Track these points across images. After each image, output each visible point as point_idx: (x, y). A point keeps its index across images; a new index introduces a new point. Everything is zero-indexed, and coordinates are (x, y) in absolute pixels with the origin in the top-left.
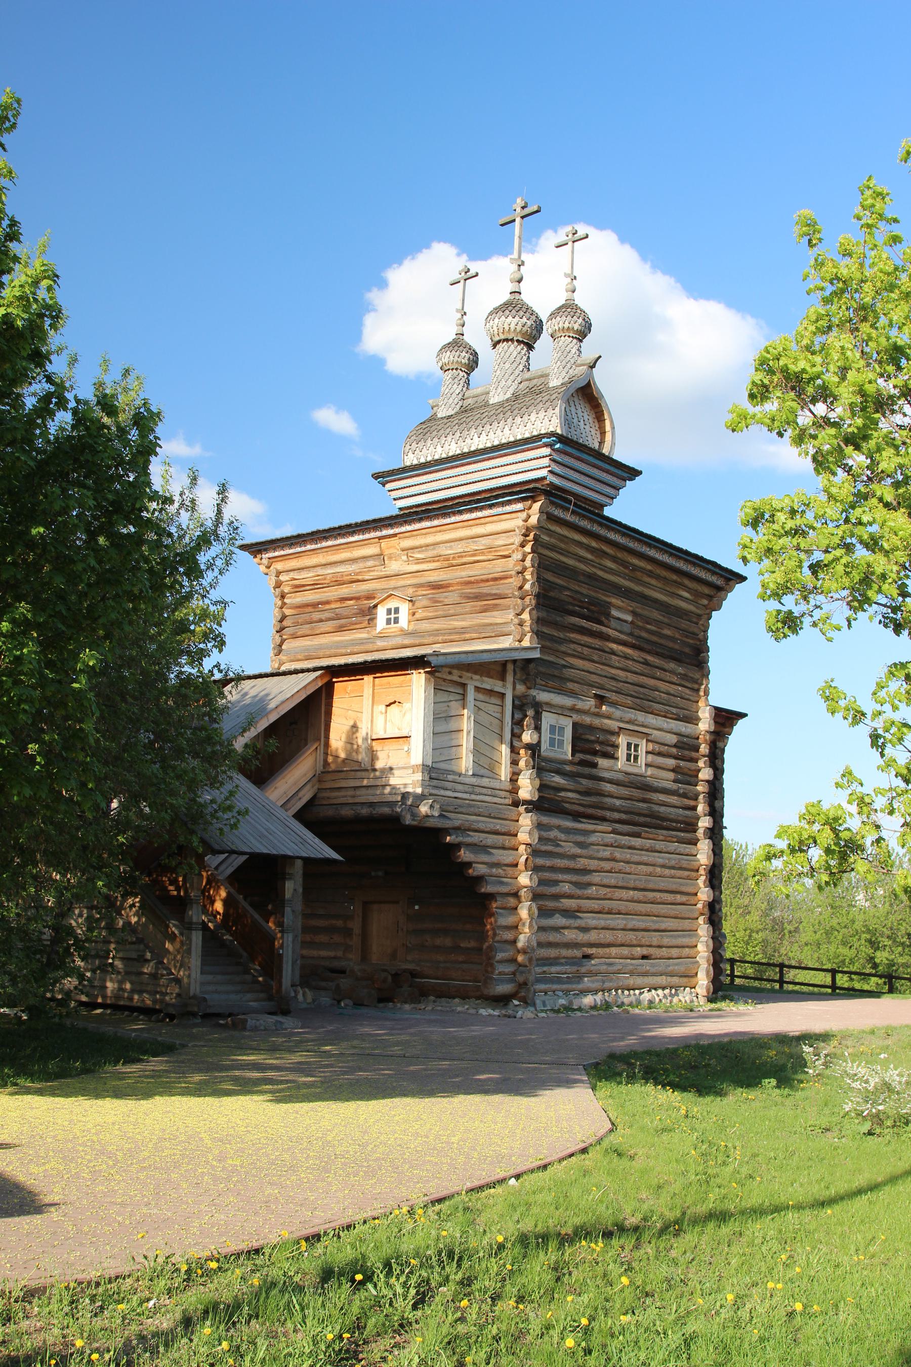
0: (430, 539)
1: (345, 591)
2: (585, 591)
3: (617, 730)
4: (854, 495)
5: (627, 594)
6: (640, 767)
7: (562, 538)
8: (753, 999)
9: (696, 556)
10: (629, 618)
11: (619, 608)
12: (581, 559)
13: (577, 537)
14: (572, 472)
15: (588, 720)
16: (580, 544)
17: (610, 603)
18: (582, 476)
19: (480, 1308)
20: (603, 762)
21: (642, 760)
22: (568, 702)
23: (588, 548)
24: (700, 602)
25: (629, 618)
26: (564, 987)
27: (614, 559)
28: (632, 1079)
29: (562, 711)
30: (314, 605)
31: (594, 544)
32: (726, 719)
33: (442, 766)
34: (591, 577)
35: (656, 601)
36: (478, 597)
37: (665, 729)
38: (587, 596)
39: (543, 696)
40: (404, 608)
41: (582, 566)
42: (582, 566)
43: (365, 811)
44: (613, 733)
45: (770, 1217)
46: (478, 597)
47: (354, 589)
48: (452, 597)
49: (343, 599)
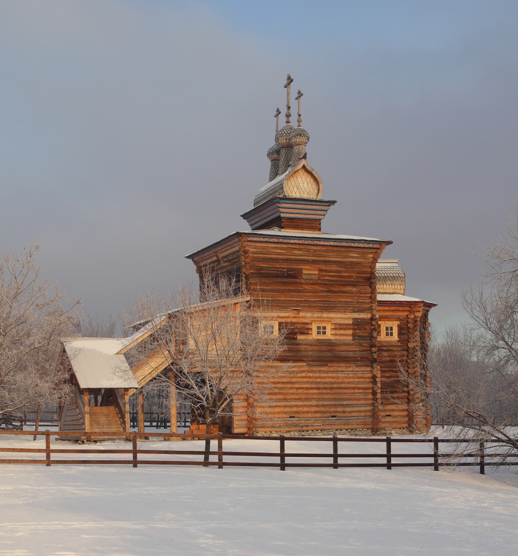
0: (314, 207)
2: (285, 267)
3: (310, 322)
5: (307, 262)
6: (329, 335)
7: (263, 248)
8: (276, 309)
9: (198, 252)
10: (317, 272)
11: (306, 269)
14: (294, 210)
17: (302, 268)
18: (301, 210)
19: (209, 313)
23: (282, 249)
25: (317, 272)
26: (276, 429)
27: (300, 250)
31: (284, 246)
34: (287, 260)
38: (285, 268)
41: (280, 257)
42: (280, 257)
44: (307, 324)
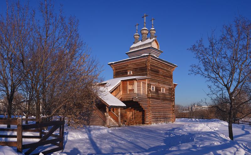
1: (123, 70)
4: (97, 75)
5: (162, 69)
12: (156, 64)
13: (155, 61)
15: (157, 86)
16: (155, 62)
20: (159, 92)
21: (164, 91)
22: (155, 84)
23: (156, 63)
24: (82, 131)
28: (174, 98)
29: (154, 85)
30: (119, 72)
32: (175, 85)
33: (139, 93)
34: (157, 67)
35: (165, 70)
36: (142, 70)
37: (167, 87)
39: (151, 83)
40: (132, 72)
41: (156, 65)
42: (156, 65)
43: (128, 100)
45: (197, 62)
46: (142, 70)
47: (124, 69)
48: (138, 70)
49: (123, 71)
